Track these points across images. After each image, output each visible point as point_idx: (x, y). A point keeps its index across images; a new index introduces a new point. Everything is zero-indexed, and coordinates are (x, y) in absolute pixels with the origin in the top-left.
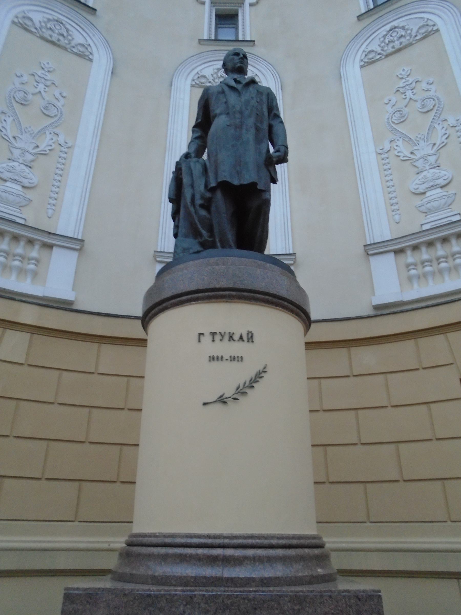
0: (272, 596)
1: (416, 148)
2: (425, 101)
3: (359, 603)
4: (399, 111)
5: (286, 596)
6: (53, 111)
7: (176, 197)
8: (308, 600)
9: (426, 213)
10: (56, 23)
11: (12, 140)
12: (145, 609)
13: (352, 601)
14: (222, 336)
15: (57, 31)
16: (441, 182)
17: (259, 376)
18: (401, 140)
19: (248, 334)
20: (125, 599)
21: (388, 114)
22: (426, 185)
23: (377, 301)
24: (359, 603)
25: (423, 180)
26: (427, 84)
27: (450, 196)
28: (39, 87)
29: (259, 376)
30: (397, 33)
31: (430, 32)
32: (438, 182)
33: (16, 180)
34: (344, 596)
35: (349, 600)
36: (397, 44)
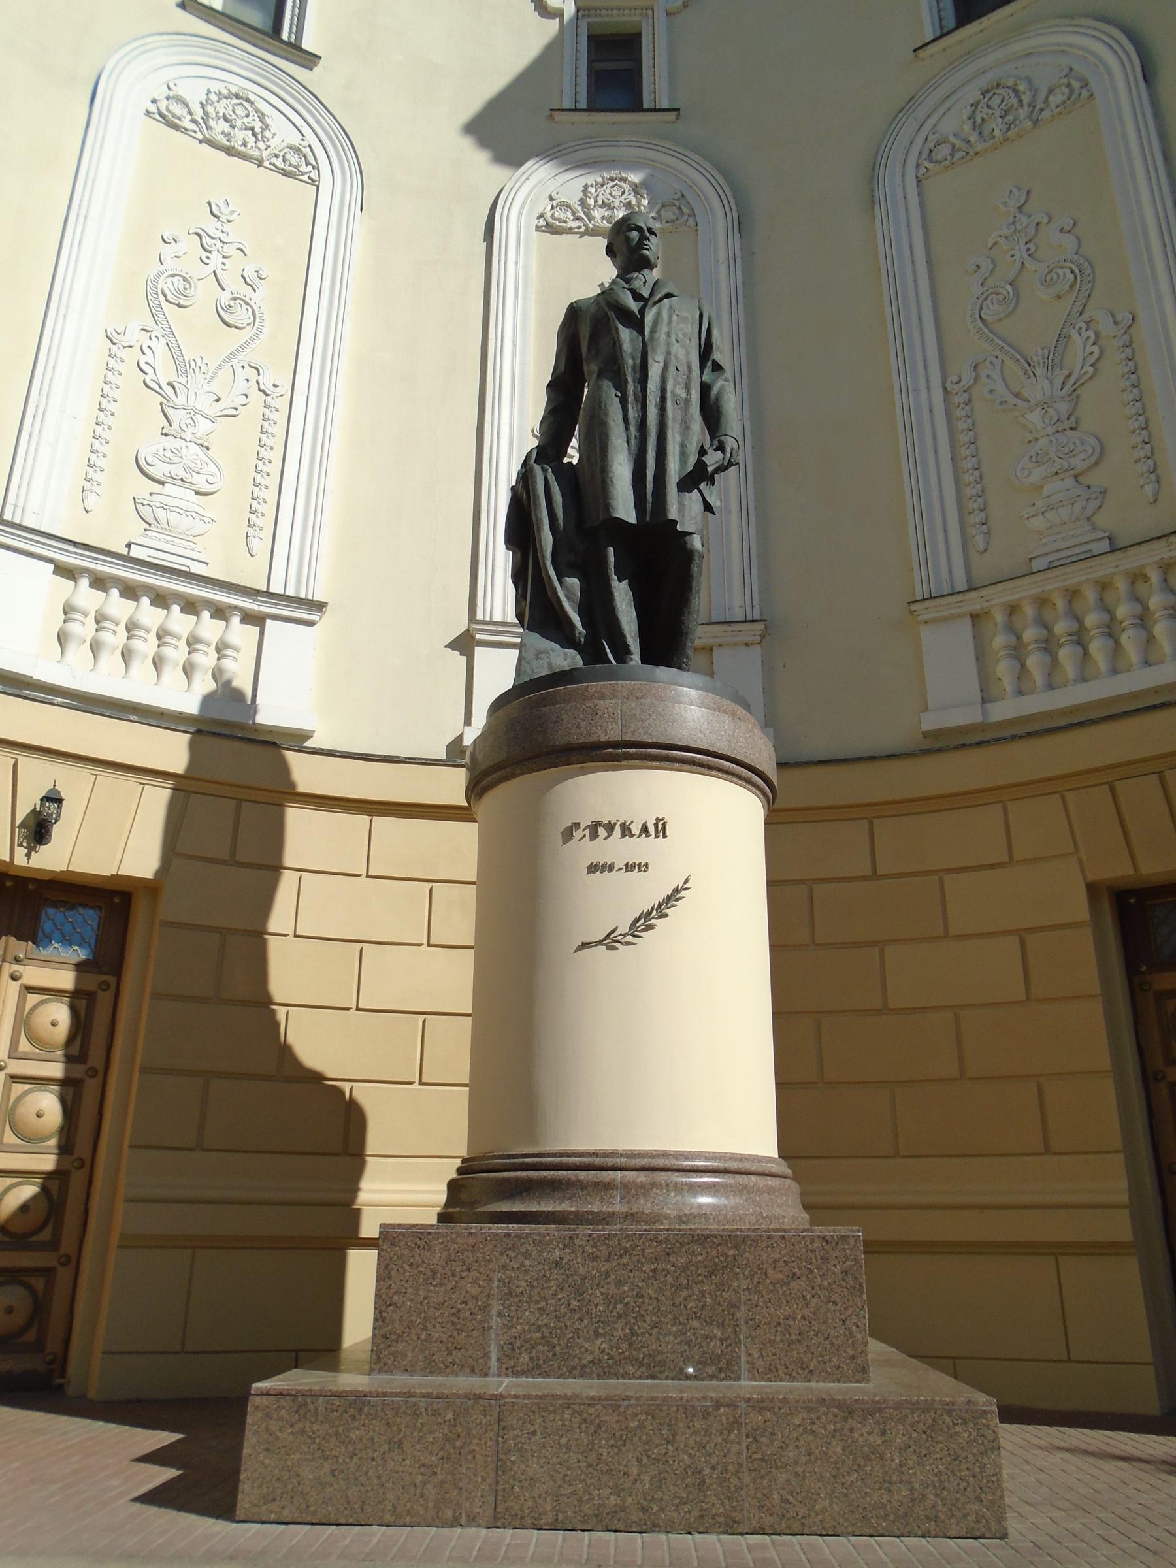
0: (693, 1236)
1: (183, 380)
3: (826, 1247)
4: (185, 280)
5: (715, 1236)
6: (241, 315)
7: (520, 532)
8: (749, 1242)
10: (235, 101)
11: (169, 390)
12: (501, 1254)
13: (817, 1244)
14: (610, 828)
15: (239, 123)
16: (201, 483)
17: (671, 899)
18: (163, 341)
19: (656, 825)
20: (471, 1241)
21: (161, 268)
23: (930, 722)
24: (826, 1247)
26: (1061, 230)
28: (212, 262)
29: (671, 899)
30: (247, 116)
33: (182, 480)
34: (804, 1237)
35: (812, 1243)
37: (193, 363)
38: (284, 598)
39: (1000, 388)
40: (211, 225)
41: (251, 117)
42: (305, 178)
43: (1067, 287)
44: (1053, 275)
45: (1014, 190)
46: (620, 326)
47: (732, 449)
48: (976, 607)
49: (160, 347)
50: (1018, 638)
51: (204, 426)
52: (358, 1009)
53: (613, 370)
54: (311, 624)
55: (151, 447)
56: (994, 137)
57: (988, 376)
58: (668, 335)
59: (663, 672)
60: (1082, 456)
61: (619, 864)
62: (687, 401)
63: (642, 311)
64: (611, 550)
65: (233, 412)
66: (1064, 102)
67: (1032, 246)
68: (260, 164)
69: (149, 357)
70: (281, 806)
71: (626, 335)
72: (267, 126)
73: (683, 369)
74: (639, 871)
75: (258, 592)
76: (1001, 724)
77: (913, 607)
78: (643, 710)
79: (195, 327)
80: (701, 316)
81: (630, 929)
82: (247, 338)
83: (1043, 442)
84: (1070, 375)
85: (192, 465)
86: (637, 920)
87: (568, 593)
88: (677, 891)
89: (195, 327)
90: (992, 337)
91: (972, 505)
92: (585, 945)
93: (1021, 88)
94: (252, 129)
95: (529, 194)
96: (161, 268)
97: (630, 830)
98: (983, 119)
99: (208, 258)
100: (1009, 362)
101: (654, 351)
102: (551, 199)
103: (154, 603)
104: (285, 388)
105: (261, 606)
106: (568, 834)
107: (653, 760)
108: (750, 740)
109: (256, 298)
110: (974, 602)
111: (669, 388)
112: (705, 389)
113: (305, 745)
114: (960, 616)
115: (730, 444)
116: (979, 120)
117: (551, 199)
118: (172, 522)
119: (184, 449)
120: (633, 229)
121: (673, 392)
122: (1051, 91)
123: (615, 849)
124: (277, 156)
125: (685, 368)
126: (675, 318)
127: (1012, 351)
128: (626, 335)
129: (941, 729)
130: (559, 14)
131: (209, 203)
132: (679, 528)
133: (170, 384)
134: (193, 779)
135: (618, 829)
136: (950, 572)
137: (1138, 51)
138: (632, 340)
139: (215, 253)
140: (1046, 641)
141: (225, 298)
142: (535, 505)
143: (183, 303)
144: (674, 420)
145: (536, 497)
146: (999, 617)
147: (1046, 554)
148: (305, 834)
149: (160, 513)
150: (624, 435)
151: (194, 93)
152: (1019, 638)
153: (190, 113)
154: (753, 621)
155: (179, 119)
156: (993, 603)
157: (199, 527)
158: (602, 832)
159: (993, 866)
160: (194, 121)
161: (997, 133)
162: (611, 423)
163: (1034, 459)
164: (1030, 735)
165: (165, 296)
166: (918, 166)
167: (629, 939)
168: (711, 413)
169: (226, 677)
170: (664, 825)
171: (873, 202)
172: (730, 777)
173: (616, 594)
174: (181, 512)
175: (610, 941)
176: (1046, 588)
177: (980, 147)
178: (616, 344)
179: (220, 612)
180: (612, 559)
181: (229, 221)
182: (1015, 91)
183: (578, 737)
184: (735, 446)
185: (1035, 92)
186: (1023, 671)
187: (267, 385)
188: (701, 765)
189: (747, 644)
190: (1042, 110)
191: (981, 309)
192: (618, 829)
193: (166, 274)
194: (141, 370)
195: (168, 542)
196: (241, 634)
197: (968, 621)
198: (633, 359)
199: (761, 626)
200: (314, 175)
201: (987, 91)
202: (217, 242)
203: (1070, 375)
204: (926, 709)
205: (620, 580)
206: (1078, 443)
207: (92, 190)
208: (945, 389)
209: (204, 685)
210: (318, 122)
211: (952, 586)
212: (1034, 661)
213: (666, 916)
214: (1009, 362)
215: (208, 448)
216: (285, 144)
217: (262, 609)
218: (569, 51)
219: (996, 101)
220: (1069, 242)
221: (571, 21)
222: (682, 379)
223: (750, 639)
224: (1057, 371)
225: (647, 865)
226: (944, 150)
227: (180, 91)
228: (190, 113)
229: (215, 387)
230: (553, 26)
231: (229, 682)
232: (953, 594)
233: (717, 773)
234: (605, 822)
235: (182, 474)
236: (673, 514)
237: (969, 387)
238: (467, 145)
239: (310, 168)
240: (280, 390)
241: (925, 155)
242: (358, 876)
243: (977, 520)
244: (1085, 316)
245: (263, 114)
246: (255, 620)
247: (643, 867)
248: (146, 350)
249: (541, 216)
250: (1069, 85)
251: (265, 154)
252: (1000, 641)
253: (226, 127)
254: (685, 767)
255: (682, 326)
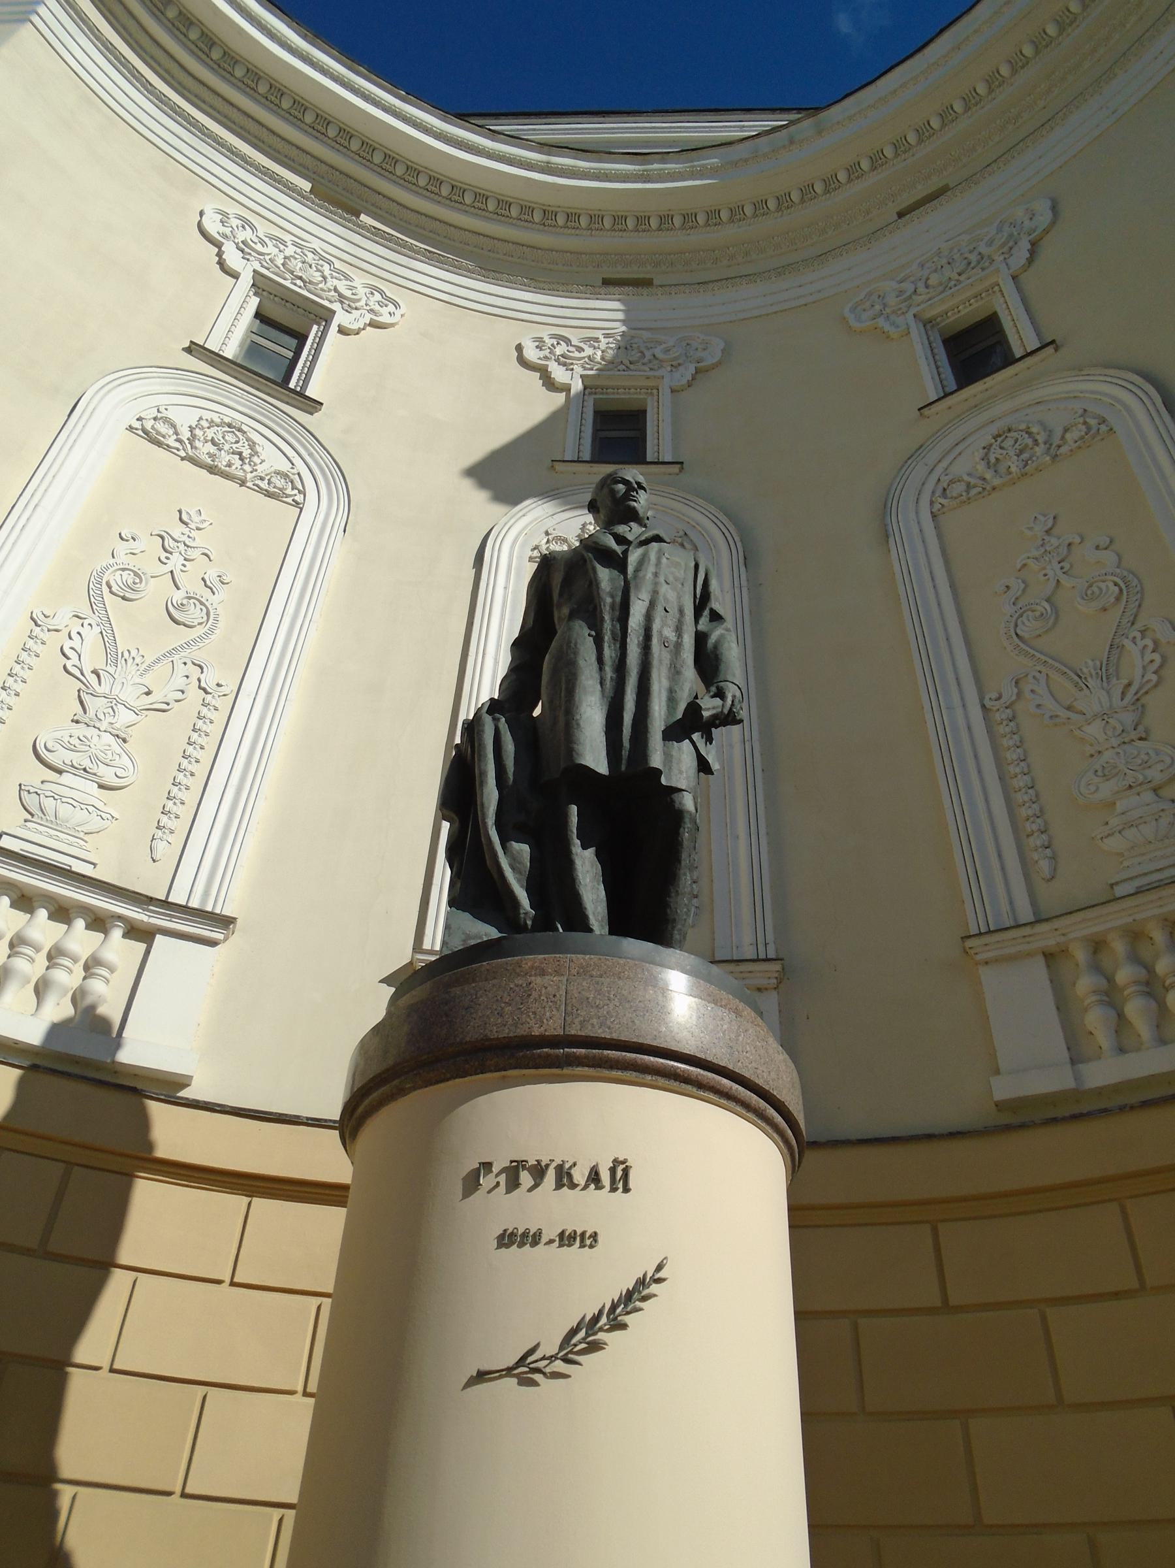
1: (111, 670)
2: (192, 601)
4: (136, 574)
6: (194, 614)
9: (32, 815)
10: (227, 429)
11: (93, 679)
14: (539, 1172)
16: (109, 777)
17: (635, 1296)
18: (97, 630)
19: (613, 1170)
21: (112, 561)
22: (68, 756)
23: (1004, 1089)
25: (75, 741)
27: (104, 815)
29: (635, 1296)
30: (237, 442)
31: (288, 496)
32: (102, 770)
33: (85, 770)
36: (223, 459)
37: (126, 655)
38: (185, 910)
39: (1049, 703)
40: (177, 530)
41: (240, 444)
42: (289, 500)
43: (1112, 600)
44: (1094, 588)
45: (1039, 517)
46: (598, 566)
47: (734, 697)
48: (1051, 942)
49: (92, 635)
50: (1109, 981)
51: (124, 717)
52: (184, 1495)
53: (589, 612)
54: (213, 943)
55: (54, 731)
56: (1010, 473)
57: (1032, 691)
58: (656, 575)
59: (633, 946)
60: (1160, 767)
61: (551, 1233)
62: (678, 645)
63: (625, 553)
64: (574, 809)
65: (164, 707)
66: (1082, 438)
67: (1066, 565)
68: (243, 483)
69: (76, 642)
70: (127, 1179)
71: (605, 576)
72: (257, 453)
73: (673, 611)
74: (582, 1246)
75: (151, 900)
76: (1099, 1092)
77: (969, 943)
78: (599, 992)
79: (139, 625)
80: (697, 567)
81: (561, 1348)
82: (195, 636)
83: (1108, 755)
84: (1129, 685)
85: (101, 755)
86: (574, 1332)
87: (513, 863)
88: (642, 1283)
89: (139, 625)
90: (1032, 652)
91: (1029, 827)
92: (482, 1376)
93: (1034, 430)
94: (240, 454)
95: (524, 529)
96: (112, 561)
97: (570, 1176)
98: (997, 459)
99: (167, 558)
100: (1054, 676)
101: (638, 588)
102: (547, 533)
103: (14, 905)
104: (230, 687)
105: (149, 917)
106: (472, 1183)
107: (611, 1068)
108: (762, 1052)
109: (213, 600)
110: (1046, 936)
111: (656, 626)
112: (701, 639)
113: (181, 1094)
114: (1030, 955)
115: (731, 691)
116: (993, 460)
117: (547, 533)
118: (61, 814)
119: (95, 739)
120: (619, 482)
121: (660, 632)
122: (1066, 430)
123: (547, 1208)
124: (262, 479)
125: (676, 610)
126: (664, 560)
127: (1057, 664)
128: (605, 576)
129: (1019, 1098)
130: (566, 389)
131: (180, 512)
132: (664, 781)
133: (95, 672)
134: (15, 1131)
135: (551, 1174)
136: (1011, 903)
137: (1153, 385)
138: (611, 580)
139: (176, 555)
140: (1147, 984)
141: (178, 596)
142: (480, 755)
143: (127, 595)
144: (660, 661)
145: (482, 746)
146: (1080, 955)
147: (1131, 879)
148: (157, 1218)
149: (49, 804)
150: (597, 676)
151: (185, 418)
152: (1110, 980)
153: (176, 433)
154: (767, 960)
155: (164, 437)
156: (1071, 936)
157: (95, 823)
158: (526, 1178)
159: (1116, 1295)
160: (179, 441)
161: (1013, 469)
162: (581, 663)
163: (1100, 773)
164: (1145, 1104)
165: (110, 587)
166: (932, 503)
167: (559, 1366)
168: (708, 663)
169: (89, 1000)
170: (626, 1172)
171: (887, 536)
172: (732, 1105)
173: (578, 863)
174: (75, 804)
175: (525, 1369)
176: (1138, 917)
177: (997, 482)
178: (593, 583)
179: (99, 922)
180: (574, 819)
181: (198, 529)
182: (1029, 433)
183: (499, 1030)
184: (738, 694)
185: (1050, 433)
186: (1121, 1022)
187: (210, 684)
188: (685, 1079)
189: (759, 990)
190: (1059, 446)
191: (1016, 625)
192: (551, 1174)
193: (116, 567)
194: (64, 654)
195: (51, 837)
196: (119, 950)
197: (1040, 961)
198: (612, 597)
199: (777, 966)
200: (299, 498)
201: (1000, 436)
202: (182, 546)
203: (1129, 685)
204: (997, 1072)
205: (584, 847)
206: (1150, 752)
207: (51, 483)
208: (983, 706)
209: (58, 1009)
210: (310, 455)
211: (1015, 920)
212: (1135, 1009)
213: (624, 1326)
214: (1054, 676)
215: (124, 741)
216: (273, 469)
217: (153, 921)
218: (573, 417)
219: (1009, 443)
220: (1109, 557)
221: (577, 395)
222: (672, 621)
223: (763, 982)
224: (1114, 681)
225: (594, 1236)
226: (959, 488)
227: (170, 414)
228: (176, 433)
229: (148, 680)
230: (560, 399)
231: (92, 1008)
232: (1018, 926)
233: (711, 1096)
234: (532, 1162)
235: (86, 763)
236: (656, 761)
237: (1012, 704)
238: (467, 484)
239: (296, 492)
240: (224, 690)
241: (939, 492)
242: (219, 1282)
243: (1038, 843)
244: (1139, 625)
245: (254, 443)
246: (141, 934)
247: (588, 1240)
248: (74, 635)
249: (536, 548)
250: (1085, 423)
251: (249, 476)
252: (1085, 985)
253: (213, 449)
254: (661, 1081)
255: (673, 569)
